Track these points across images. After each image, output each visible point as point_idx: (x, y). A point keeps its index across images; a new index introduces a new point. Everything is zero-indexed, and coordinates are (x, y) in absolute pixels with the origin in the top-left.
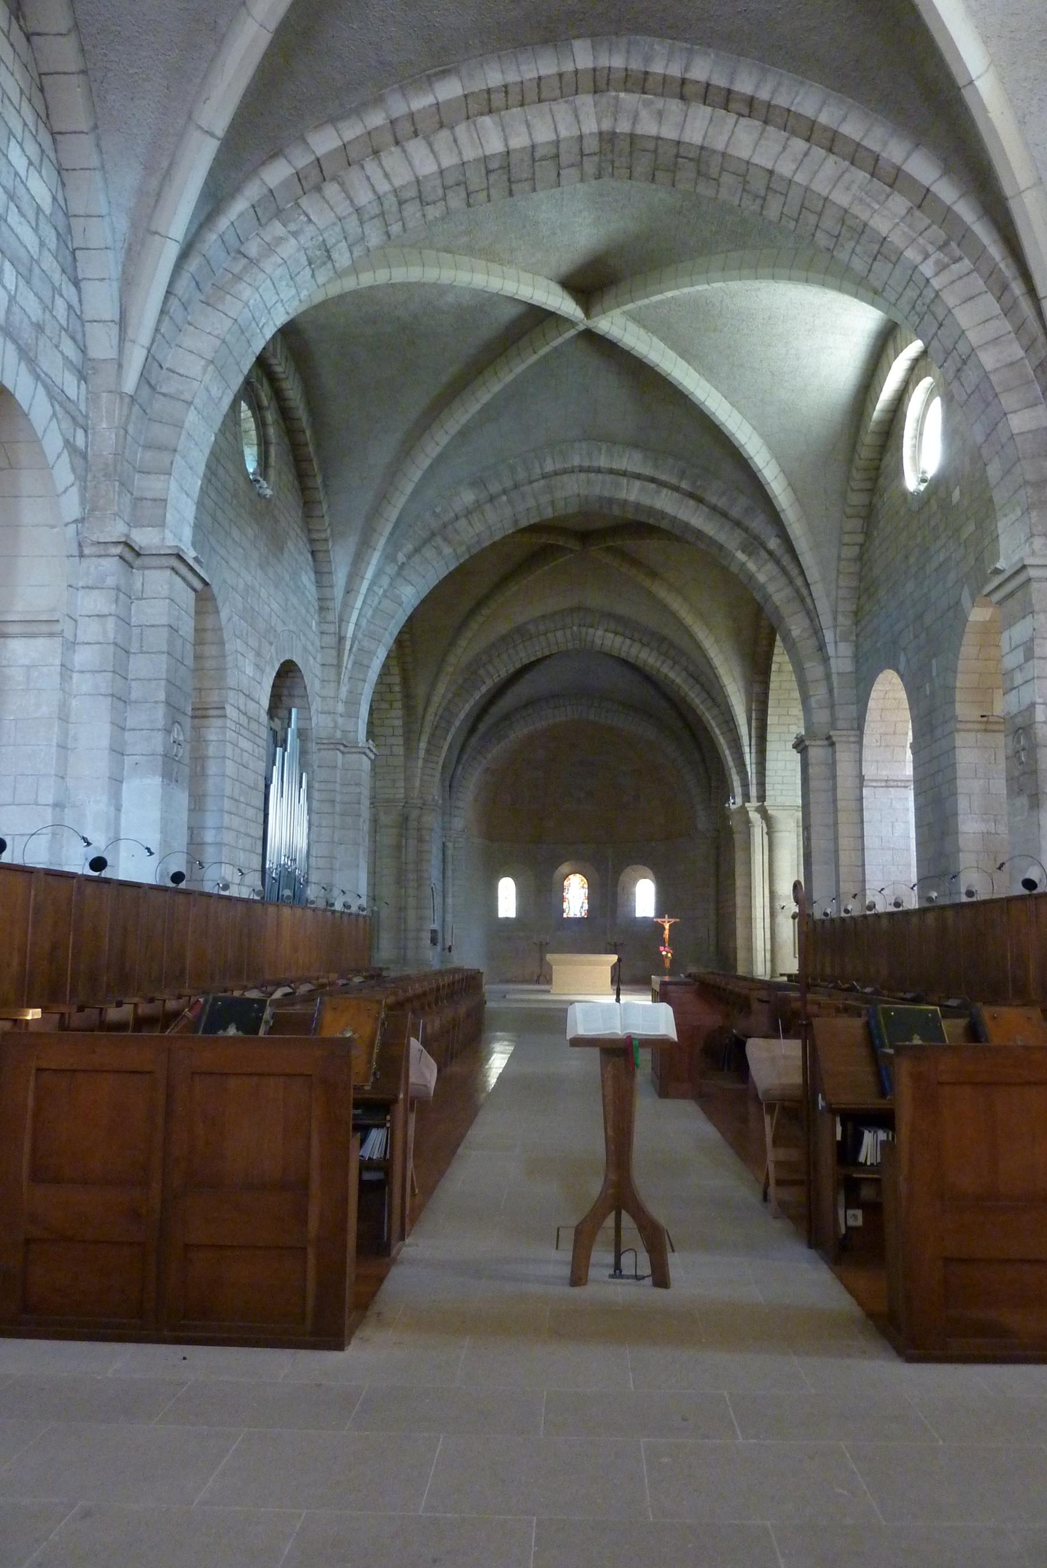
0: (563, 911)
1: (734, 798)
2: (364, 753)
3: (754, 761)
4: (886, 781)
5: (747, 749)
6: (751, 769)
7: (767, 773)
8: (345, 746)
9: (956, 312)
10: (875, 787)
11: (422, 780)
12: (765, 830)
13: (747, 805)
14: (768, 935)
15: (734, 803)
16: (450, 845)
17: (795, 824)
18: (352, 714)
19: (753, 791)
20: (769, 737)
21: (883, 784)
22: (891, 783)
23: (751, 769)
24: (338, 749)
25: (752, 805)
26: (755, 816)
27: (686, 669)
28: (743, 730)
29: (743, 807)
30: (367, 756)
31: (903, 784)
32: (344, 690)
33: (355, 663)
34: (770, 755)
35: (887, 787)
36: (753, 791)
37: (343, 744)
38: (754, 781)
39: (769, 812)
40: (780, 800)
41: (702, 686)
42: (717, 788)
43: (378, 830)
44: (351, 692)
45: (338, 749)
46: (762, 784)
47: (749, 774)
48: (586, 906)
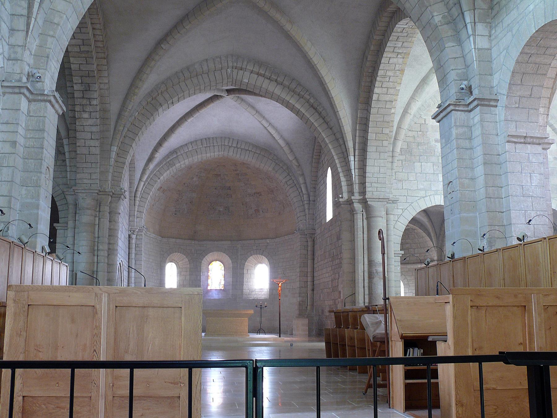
0: (208, 285)
1: (342, 194)
2: (50, 102)
3: (357, 167)
4: (525, 137)
5: (352, 158)
6: (355, 173)
7: (367, 175)
8: (31, 93)
9: (314, 123)
10: (515, 143)
11: (113, 176)
12: (365, 217)
13: (353, 198)
14: (367, 292)
15: (342, 198)
16: (134, 237)
17: (385, 212)
18: (24, 27)
19: (356, 188)
20: (369, 149)
21: (522, 140)
22: (529, 140)
23: (355, 173)
24: (24, 94)
25: (357, 197)
26: (358, 206)
27: (308, 101)
28: (350, 144)
29: (350, 198)
30: (53, 106)
31: (537, 141)
32: (34, 44)
33: (45, 21)
34: (369, 162)
35: (525, 143)
36: (356, 188)
37: (28, 89)
38: (357, 181)
39: (369, 203)
40: (376, 195)
41: (320, 114)
42: (314, 201)
43: (77, 212)
44: (41, 47)
45: (24, 94)
46: (363, 184)
47: (354, 176)
48: (223, 282)
